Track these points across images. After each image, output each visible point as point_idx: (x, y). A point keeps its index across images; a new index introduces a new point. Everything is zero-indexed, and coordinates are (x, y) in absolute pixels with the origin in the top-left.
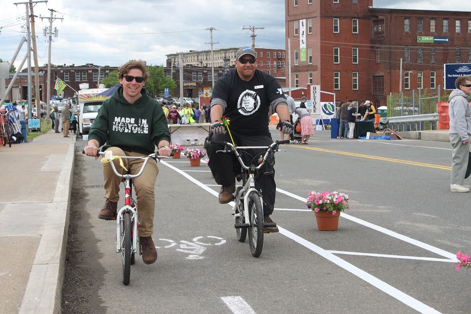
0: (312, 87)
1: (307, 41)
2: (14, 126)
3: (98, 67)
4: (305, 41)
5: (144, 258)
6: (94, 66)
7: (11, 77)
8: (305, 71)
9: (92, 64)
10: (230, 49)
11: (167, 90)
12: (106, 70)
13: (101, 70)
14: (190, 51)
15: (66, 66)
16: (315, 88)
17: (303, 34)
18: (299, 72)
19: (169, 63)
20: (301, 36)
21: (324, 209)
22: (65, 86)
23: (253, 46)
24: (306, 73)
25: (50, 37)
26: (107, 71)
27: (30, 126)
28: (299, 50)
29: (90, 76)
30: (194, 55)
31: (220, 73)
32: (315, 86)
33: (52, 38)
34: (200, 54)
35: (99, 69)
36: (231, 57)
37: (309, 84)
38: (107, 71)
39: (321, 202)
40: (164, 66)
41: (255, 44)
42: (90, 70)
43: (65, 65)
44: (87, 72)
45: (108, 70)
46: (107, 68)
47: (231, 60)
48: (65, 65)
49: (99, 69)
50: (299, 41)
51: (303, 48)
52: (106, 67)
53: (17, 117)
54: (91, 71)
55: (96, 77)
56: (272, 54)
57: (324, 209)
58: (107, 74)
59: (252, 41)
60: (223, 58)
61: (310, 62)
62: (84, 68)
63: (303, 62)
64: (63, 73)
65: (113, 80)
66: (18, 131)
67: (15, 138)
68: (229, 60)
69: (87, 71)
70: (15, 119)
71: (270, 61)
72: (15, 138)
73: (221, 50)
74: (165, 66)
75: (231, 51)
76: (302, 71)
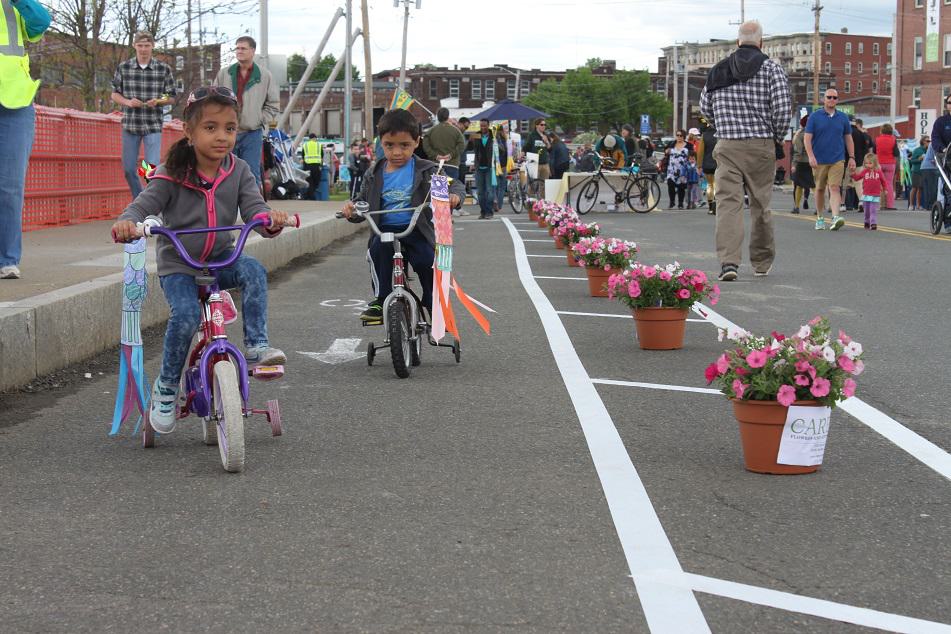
0: (918, 113)
1: (942, 16)
2: (282, 168)
3: (515, 70)
4: (937, 20)
5: (770, 610)
6: (511, 69)
7: (317, 90)
8: (934, 83)
9: (505, 66)
10: (794, 37)
11: (647, 119)
12: (532, 77)
13: (522, 77)
14: (712, 40)
15: (459, 69)
16: (924, 116)
17: (933, 6)
18: (922, 83)
19: (663, 63)
20: (929, 8)
21: (596, 263)
22: (412, 101)
23: (817, 28)
24: (938, 86)
25: (407, 9)
26: (536, 80)
27: (342, 177)
28: (925, 38)
29: (501, 88)
30: (719, 48)
31: (501, 84)
32: (924, 111)
33: (410, 11)
34: (731, 46)
35: (518, 75)
36: (795, 54)
37: (914, 106)
38: (536, 80)
39: (589, 251)
40: (650, 72)
41: (820, 24)
42: (501, 76)
43: (474, 66)
44: (461, 80)
45: (537, 77)
46: (536, 73)
47: (796, 59)
48: (474, 66)
49: (518, 75)
50: (925, 19)
51: (933, 35)
52: (534, 71)
53: (288, 150)
54: (502, 80)
55: (524, 87)
56: (855, 47)
57: (596, 263)
58: (533, 86)
59: (814, 18)
60: (779, 55)
61: (946, 64)
62: (491, 73)
63: (931, 63)
64: (470, 82)
65: (546, 98)
66: (289, 178)
67: (282, 190)
68: (792, 59)
69: (495, 78)
70: (285, 157)
71: (878, 61)
72: (282, 190)
73: (774, 39)
74: (654, 69)
75: (797, 40)
76: (928, 83)
